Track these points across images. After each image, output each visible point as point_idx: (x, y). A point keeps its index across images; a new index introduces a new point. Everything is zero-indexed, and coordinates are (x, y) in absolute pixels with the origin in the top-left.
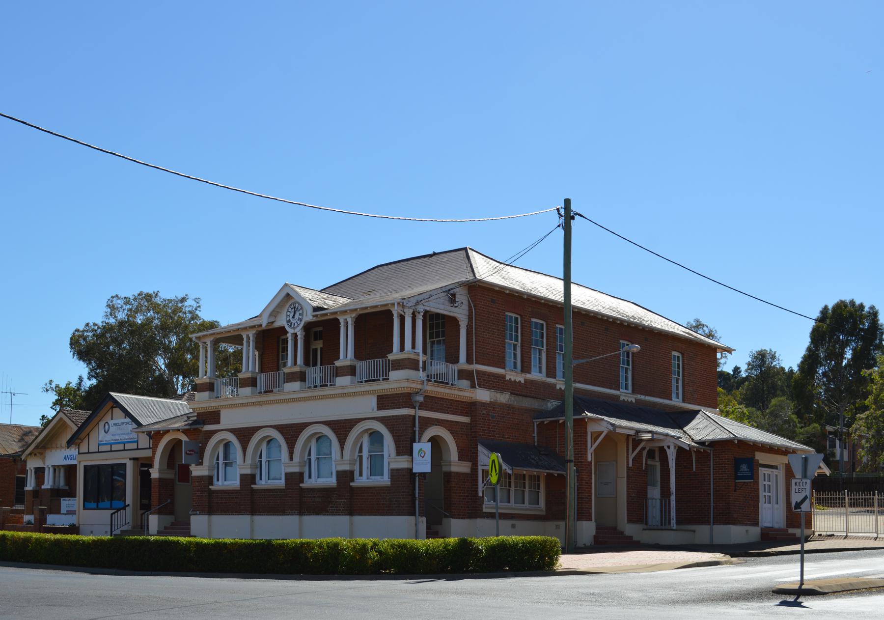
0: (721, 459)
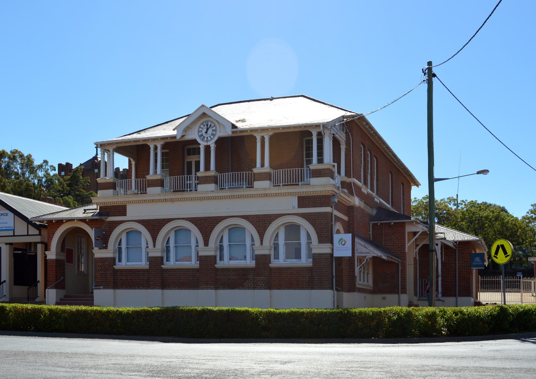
0: (463, 254)
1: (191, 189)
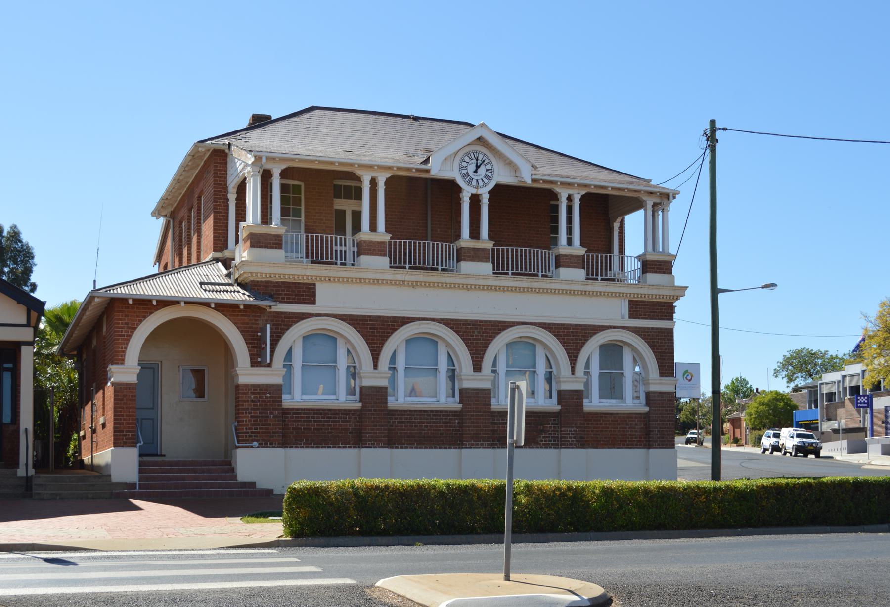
1: (343, 262)
